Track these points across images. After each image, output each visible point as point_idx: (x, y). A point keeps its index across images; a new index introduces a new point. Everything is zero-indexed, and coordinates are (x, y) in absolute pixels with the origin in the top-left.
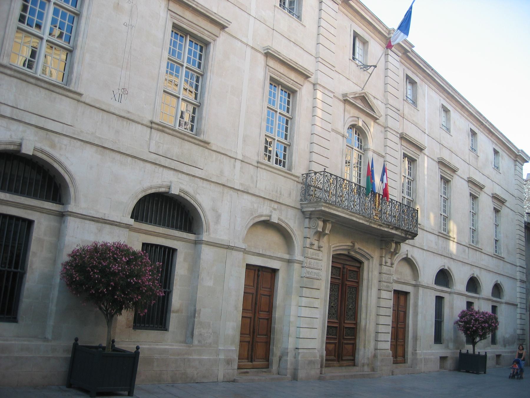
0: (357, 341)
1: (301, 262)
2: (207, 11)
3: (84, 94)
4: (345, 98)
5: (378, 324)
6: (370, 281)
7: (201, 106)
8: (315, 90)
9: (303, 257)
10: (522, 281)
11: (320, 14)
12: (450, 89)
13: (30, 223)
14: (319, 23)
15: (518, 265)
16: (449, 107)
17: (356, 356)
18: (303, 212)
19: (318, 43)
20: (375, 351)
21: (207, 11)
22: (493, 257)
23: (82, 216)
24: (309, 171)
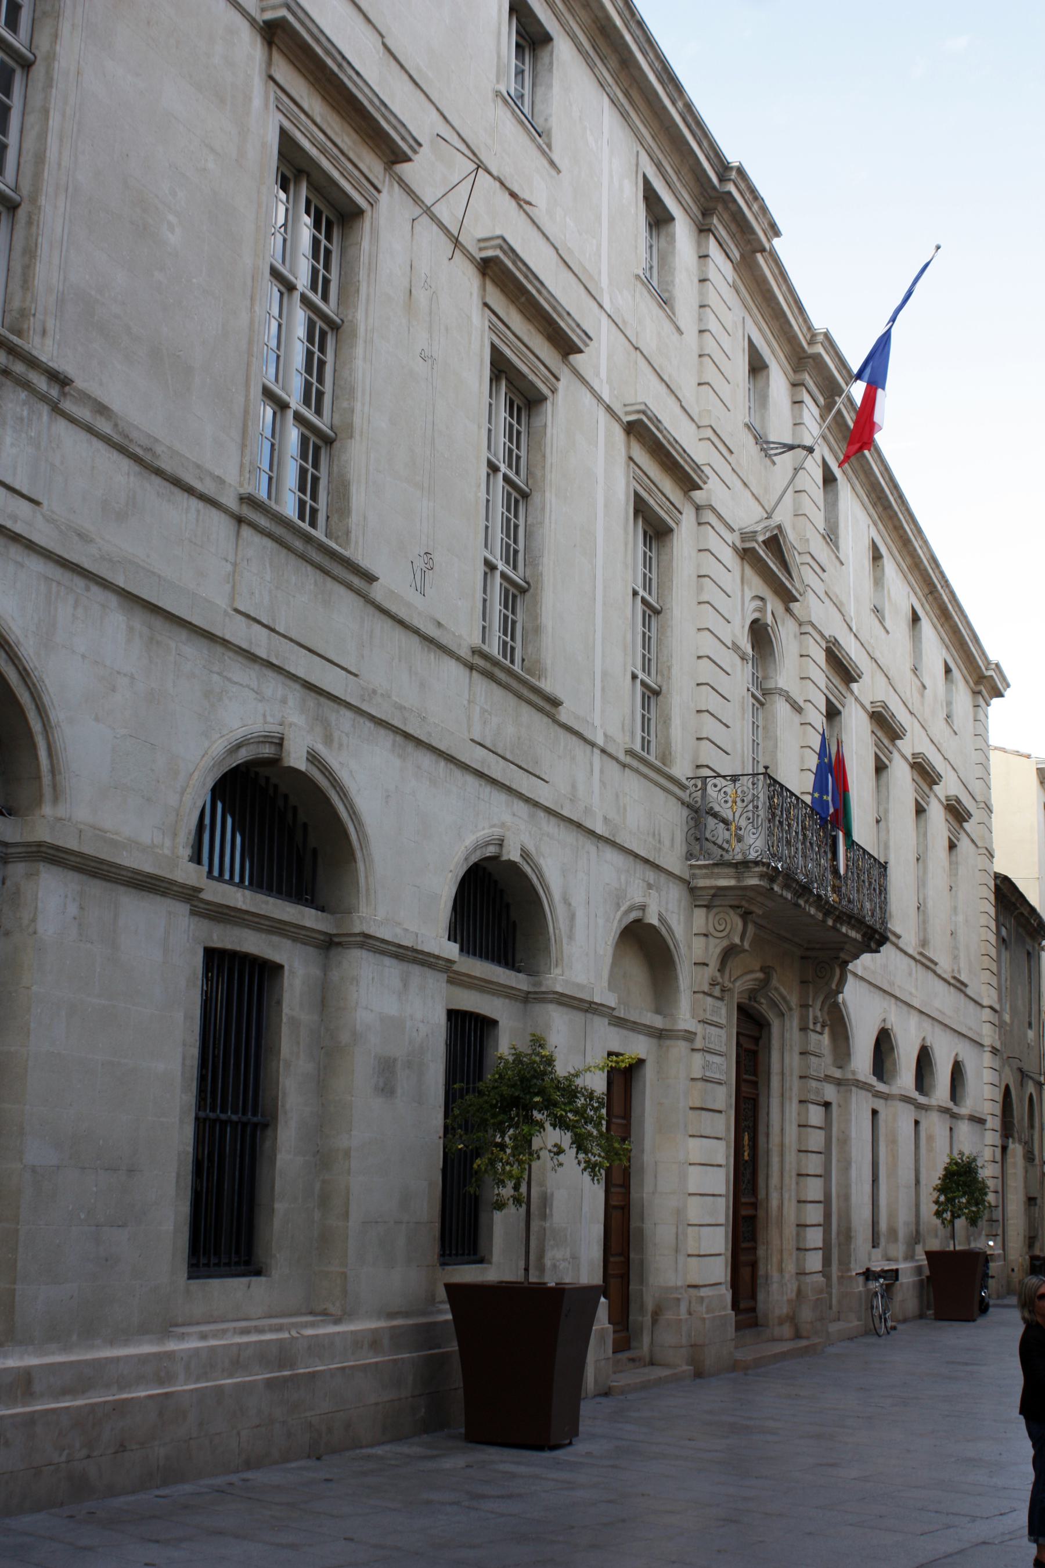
0: (761, 1252)
1: (689, 1036)
2: (554, 309)
3: (381, 578)
4: (748, 545)
5: (805, 1202)
6: (788, 1078)
7: (531, 591)
8: (699, 524)
9: (695, 1021)
10: (995, 1051)
11: (702, 294)
12: (892, 495)
13: (276, 969)
14: (700, 320)
15: (985, 1003)
16: (883, 550)
17: (761, 1296)
18: (692, 890)
19: (702, 381)
20: (797, 1280)
21: (554, 309)
22: (949, 983)
23: (382, 945)
24: (698, 767)
